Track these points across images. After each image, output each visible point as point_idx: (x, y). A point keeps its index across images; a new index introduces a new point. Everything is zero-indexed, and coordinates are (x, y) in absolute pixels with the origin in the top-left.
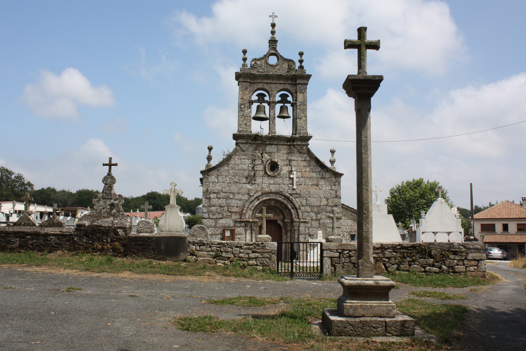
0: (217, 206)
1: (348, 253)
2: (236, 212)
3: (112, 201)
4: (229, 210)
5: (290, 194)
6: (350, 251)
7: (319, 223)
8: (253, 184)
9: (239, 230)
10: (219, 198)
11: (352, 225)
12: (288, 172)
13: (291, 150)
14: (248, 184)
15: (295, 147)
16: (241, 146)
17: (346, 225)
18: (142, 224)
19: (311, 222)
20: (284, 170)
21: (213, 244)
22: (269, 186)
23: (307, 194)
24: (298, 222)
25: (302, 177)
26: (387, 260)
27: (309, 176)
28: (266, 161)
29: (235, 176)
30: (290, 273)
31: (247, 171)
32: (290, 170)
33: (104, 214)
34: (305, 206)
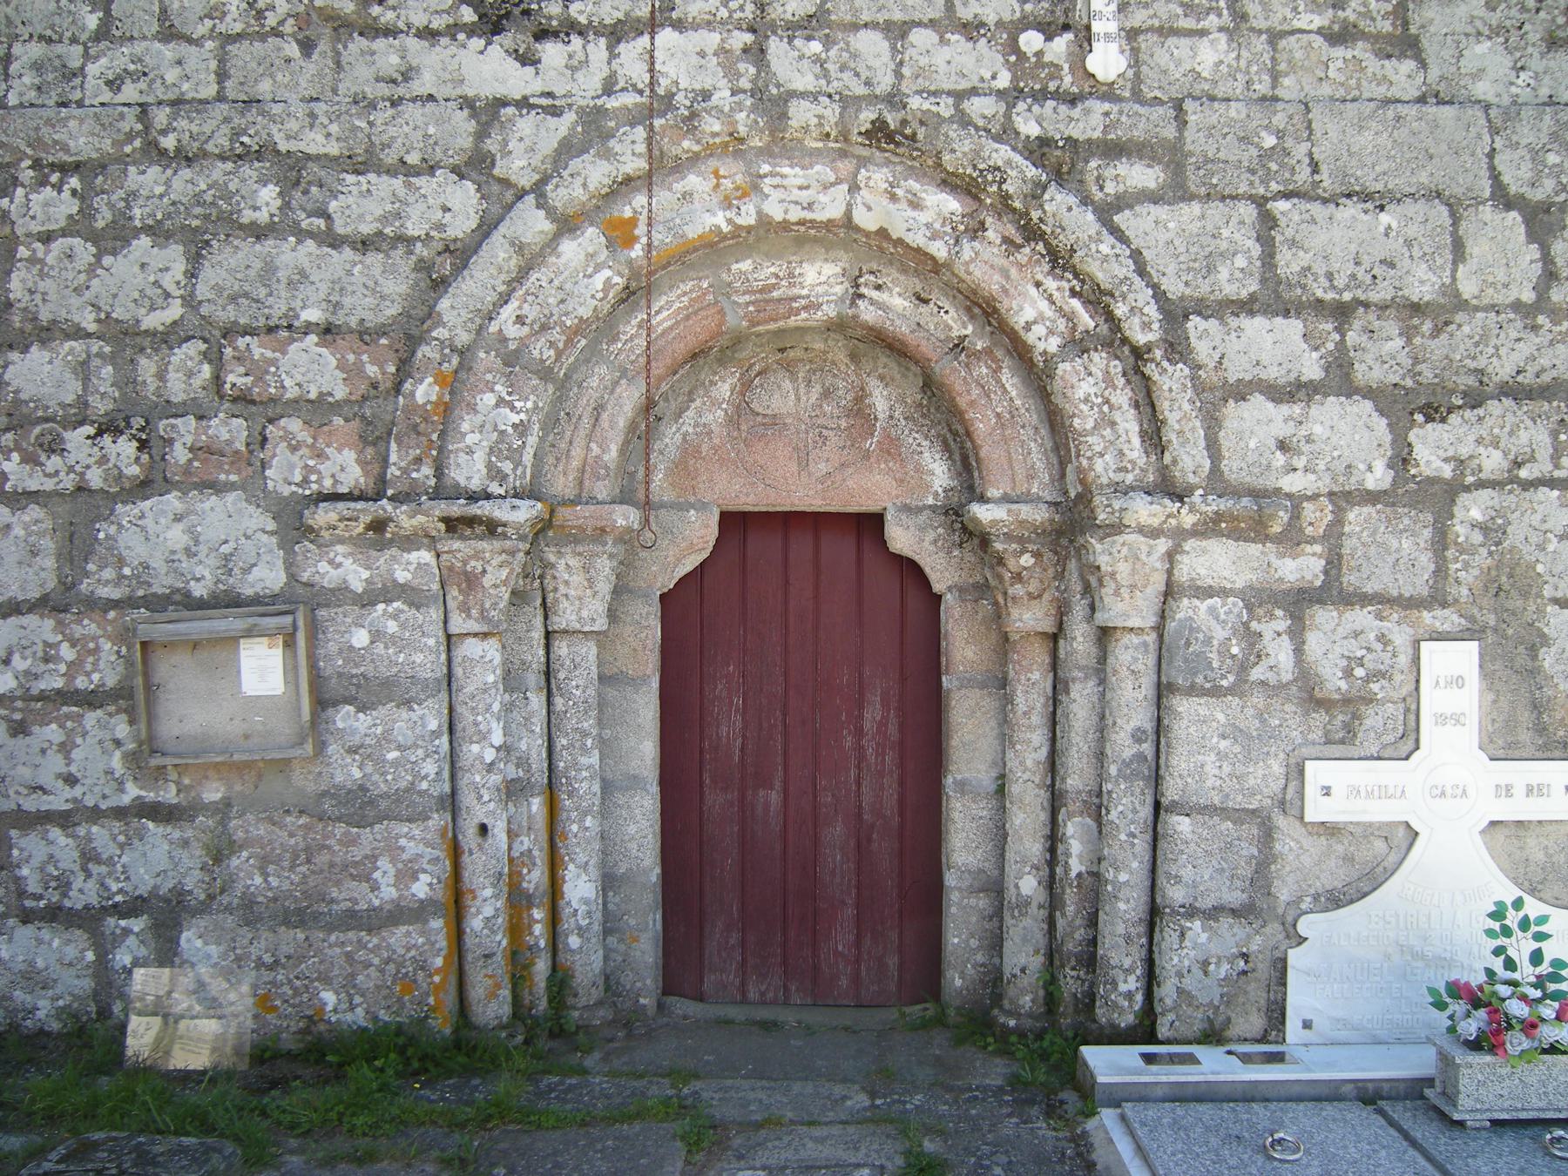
2: (318, 409)
7: (1441, 542)
8: (542, 35)
14: (477, 43)
22: (757, 53)
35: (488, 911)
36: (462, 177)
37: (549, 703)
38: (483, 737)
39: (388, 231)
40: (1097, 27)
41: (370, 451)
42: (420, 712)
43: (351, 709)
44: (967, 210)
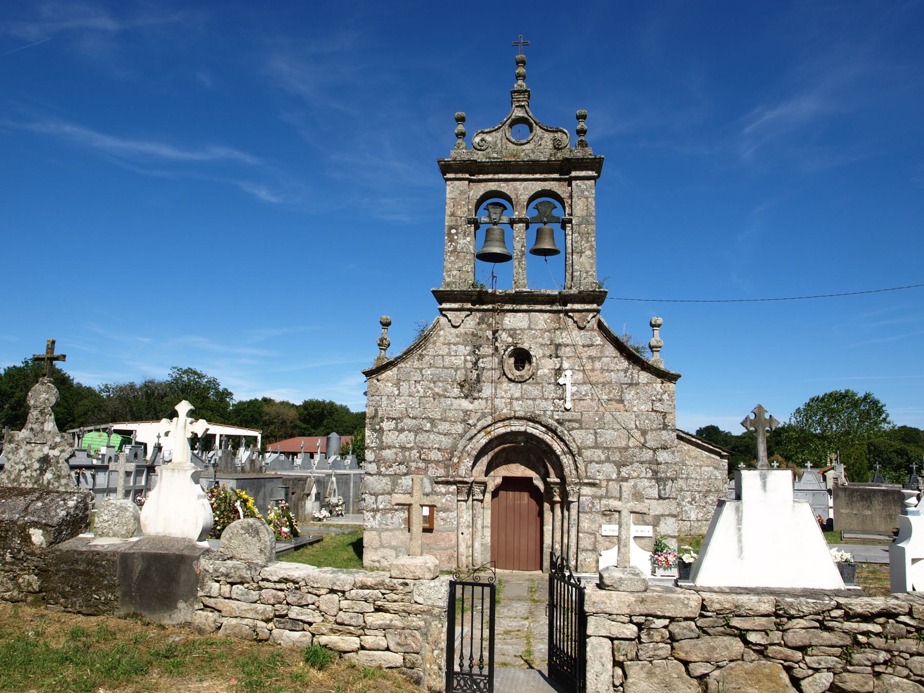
0: (395, 447)
1: (666, 627)
2: (437, 462)
3: (46, 450)
4: (423, 456)
5: (558, 421)
6: (672, 619)
10: (402, 431)
11: (711, 479)
12: (553, 372)
13: (559, 323)
14: (464, 400)
15: (570, 317)
16: (448, 315)
17: (699, 478)
18: (106, 512)
19: (607, 485)
20: (545, 367)
21: (268, 580)
22: (511, 403)
24: (576, 484)
25: (584, 383)
26: (799, 655)
27: (602, 380)
28: (504, 347)
29: (436, 381)
30: (485, 676)
31: (463, 370)
32: (558, 367)
33: (26, 483)
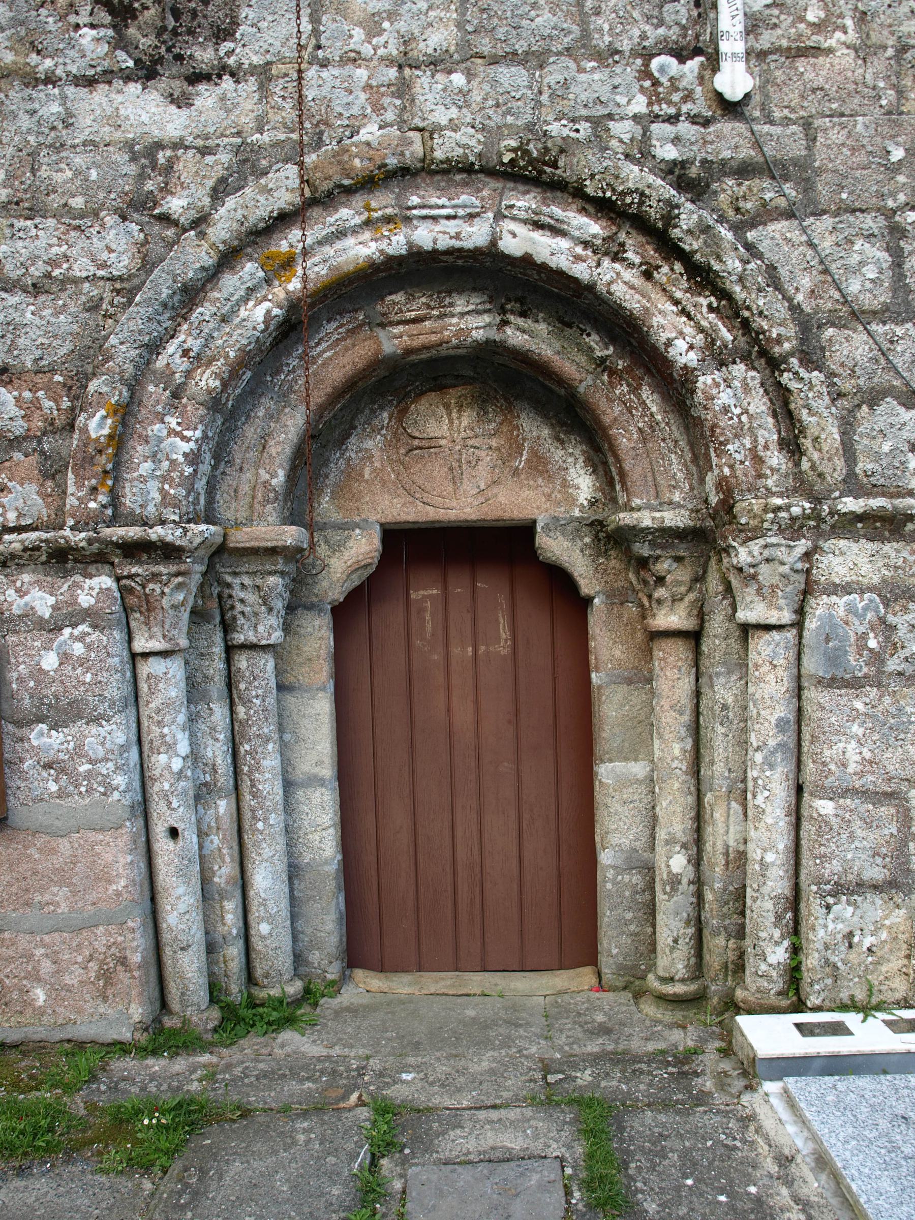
8: (195, 78)
9: (50, 661)
14: (134, 88)
22: (403, 89)
23: (894, 169)
34: (882, 314)
35: (182, 907)
36: (124, 218)
37: (232, 712)
38: (170, 748)
39: (56, 272)
40: (725, 47)
41: (49, 483)
42: (108, 728)
43: (44, 727)
44: (607, 233)
